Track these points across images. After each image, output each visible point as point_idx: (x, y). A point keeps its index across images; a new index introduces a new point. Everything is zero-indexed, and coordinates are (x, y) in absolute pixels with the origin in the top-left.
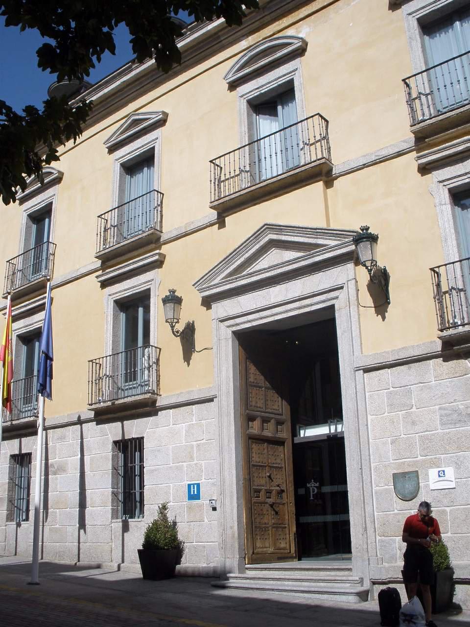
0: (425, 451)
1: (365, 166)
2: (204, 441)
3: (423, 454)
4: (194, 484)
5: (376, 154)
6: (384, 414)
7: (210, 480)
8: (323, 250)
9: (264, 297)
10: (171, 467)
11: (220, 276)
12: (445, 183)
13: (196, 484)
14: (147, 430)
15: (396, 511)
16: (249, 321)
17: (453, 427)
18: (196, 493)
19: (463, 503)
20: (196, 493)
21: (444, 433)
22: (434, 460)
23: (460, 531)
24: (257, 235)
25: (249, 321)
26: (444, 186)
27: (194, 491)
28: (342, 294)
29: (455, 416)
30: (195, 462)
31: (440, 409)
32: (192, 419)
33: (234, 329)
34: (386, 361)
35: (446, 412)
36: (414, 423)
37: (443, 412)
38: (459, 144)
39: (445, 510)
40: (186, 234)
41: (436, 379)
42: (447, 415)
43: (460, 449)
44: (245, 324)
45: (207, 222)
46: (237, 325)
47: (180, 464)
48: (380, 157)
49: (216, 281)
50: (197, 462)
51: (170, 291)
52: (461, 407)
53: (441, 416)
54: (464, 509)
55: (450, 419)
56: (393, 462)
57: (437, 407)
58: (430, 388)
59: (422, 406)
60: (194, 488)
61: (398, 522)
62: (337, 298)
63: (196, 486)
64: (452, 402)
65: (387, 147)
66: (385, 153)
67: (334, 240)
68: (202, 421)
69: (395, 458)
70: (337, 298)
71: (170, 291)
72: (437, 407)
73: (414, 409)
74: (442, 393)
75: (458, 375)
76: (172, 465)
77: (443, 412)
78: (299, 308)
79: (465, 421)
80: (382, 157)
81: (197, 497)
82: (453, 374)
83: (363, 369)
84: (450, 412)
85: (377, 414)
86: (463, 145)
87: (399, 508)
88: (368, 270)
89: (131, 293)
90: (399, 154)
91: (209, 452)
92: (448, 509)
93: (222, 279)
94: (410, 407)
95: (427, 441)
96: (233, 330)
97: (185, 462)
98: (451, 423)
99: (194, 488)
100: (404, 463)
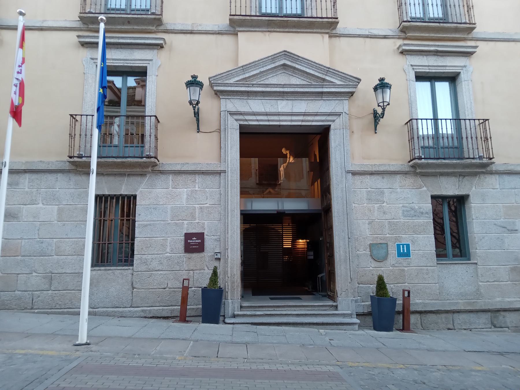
0: (392, 232)
1: (359, 36)
2: (207, 205)
3: (390, 232)
4: (403, 245)
5: (370, 31)
6: (364, 204)
7: (213, 237)
8: (329, 85)
9: (272, 105)
10: (168, 224)
11: (236, 78)
12: (415, 67)
13: (405, 244)
14: (140, 189)
15: (371, 268)
16: (258, 120)
17: (411, 218)
18: (405, 251)
19: (416, 265)
20: (405, 251)
21: (405, 222)
22: (398, 237)
23: (413, 282)
24: (274, 58)
25: (258, 120)
26: (413, 69)
27: (403, 250)
28: (338, 119)
29: (412, 212)
30: (197, 221)
31: (403, 206)
32: (195, 186)
33: (242, 123)
34: (370, 170)
35: (407, 209)
36: (384, 213)
37: (405, 209)
38: (432, 46)
39: (405, 269)
40: (191, 32)
41: (401, 188)
42: (407, 211)
43: (415, 232)
44: (253, 121)
45: (217, 30)
46: (246, 120)
47: (180, 221)
48: (372, 34)
49: (232, 81)
50: (199, 221)
51: (193, 77)
52: (417, 207)
53: (403, 211)
54: (416, 269)
55: (409, 213)
56: (369, 236)
57: (401, 205)
58: (397, 192)
59: (391, 203)
60: (403, 247)
61: (373, 275)
62: (334, 121)
63: (405, 246)
64: (411, 204)
65: (378, 29)
66: (376, 32)
67: (340, 80)
68: (206, 189)
69: (371, 234)
70: (334, 121)
71: (193, 77)
72: (401, 205)
73: (385, 204)
74: (405, 197)
75: (415, 188)
76: (170, 222)
77: (405, 209)
78: (302, 121)
79: (419, 216)
80: (374, 34)
81: (200, 248)
82: (412, 187)
83: (352, 173)
84: (409, 209)
85: (359, 203)
86: (434, 48)
87: (373, 266)
88: (382, 108)
89: (122, 64)
90: (385, 37)
91: (212, 214)
92: (406, 269)
93: (237, 81)
94: (383, 202)
95: (393, 225)
96: (240, 123)
97: (185, 220)
98: (409, 216)
99: (403, 247)
100: (377, 237)
